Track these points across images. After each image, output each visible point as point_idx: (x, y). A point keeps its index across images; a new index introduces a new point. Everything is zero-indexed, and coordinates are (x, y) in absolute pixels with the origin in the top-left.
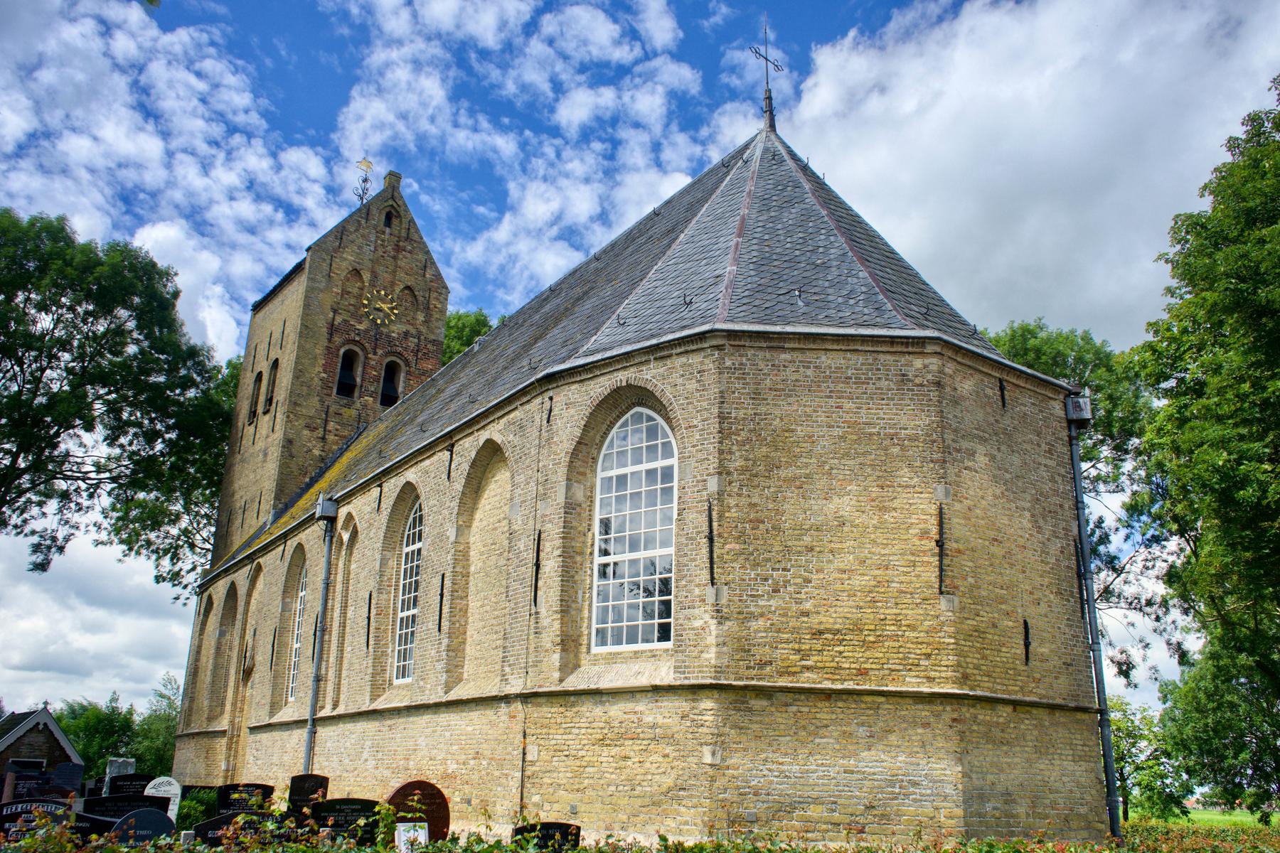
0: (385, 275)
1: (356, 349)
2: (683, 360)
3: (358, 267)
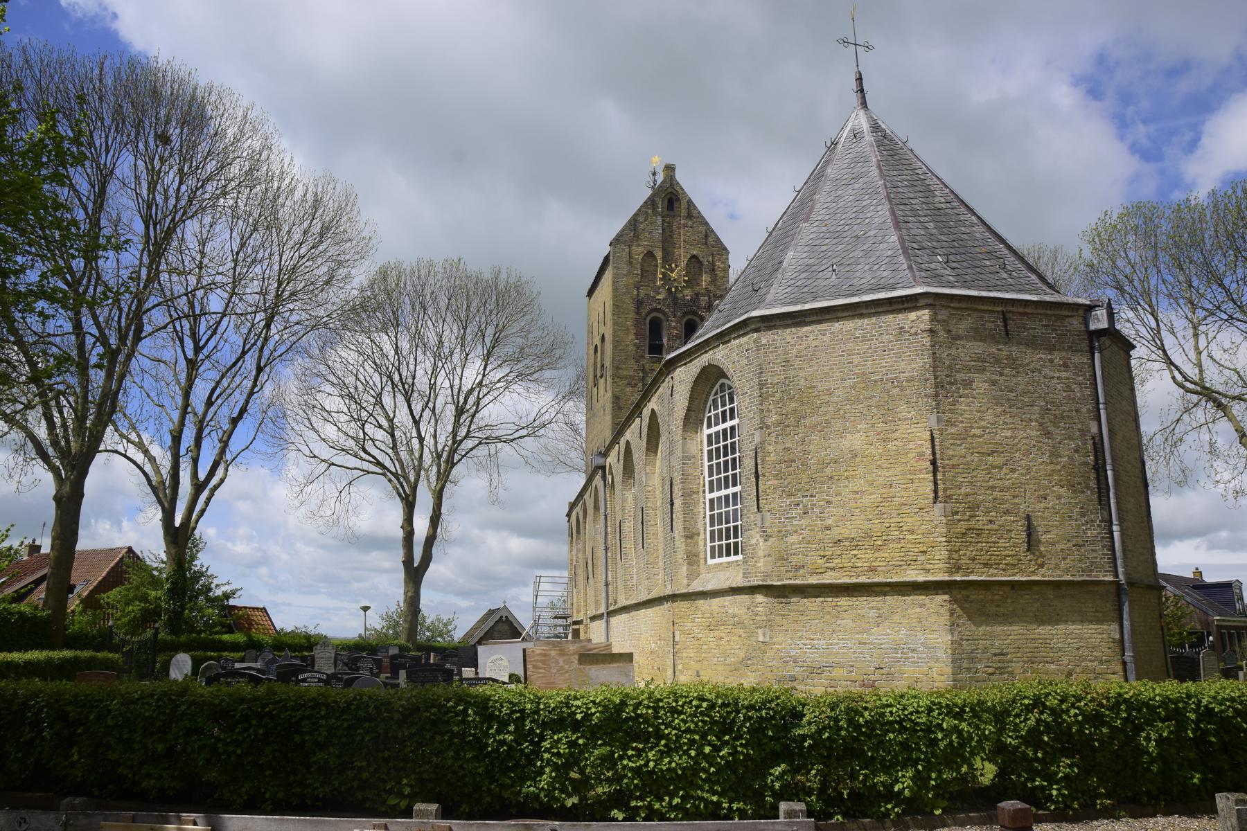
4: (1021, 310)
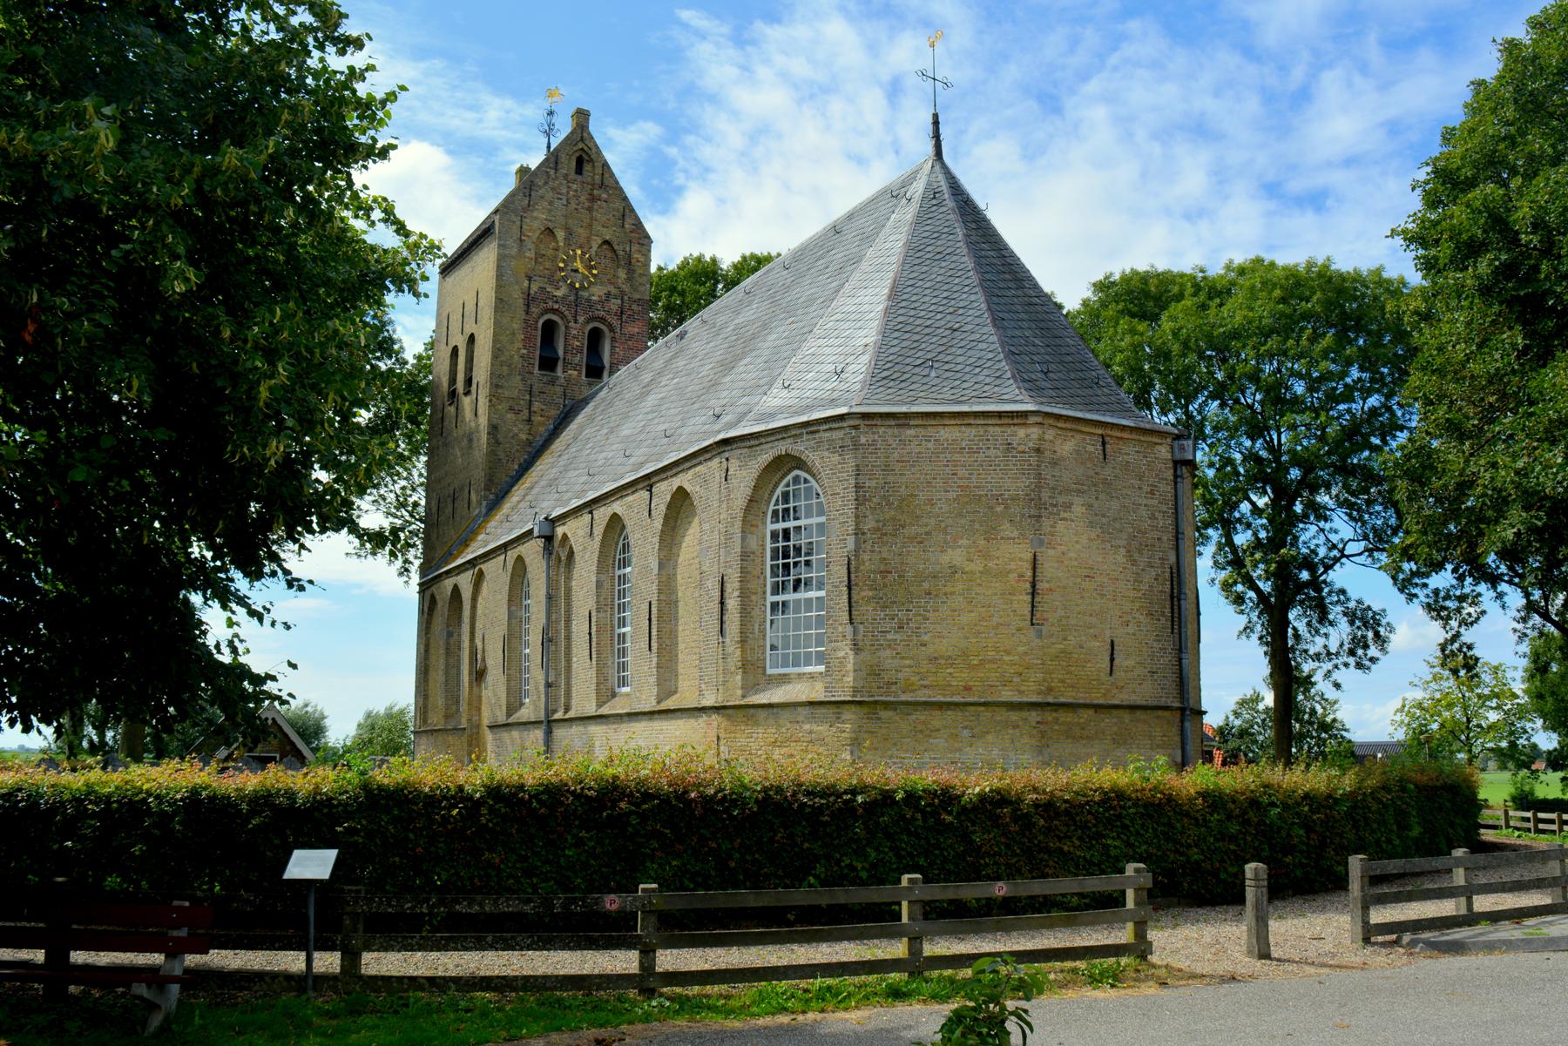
0: (581, 231)
1: (554, 318)
2: (827, 434)
3: (551, 225)
4: (1119, 434)
